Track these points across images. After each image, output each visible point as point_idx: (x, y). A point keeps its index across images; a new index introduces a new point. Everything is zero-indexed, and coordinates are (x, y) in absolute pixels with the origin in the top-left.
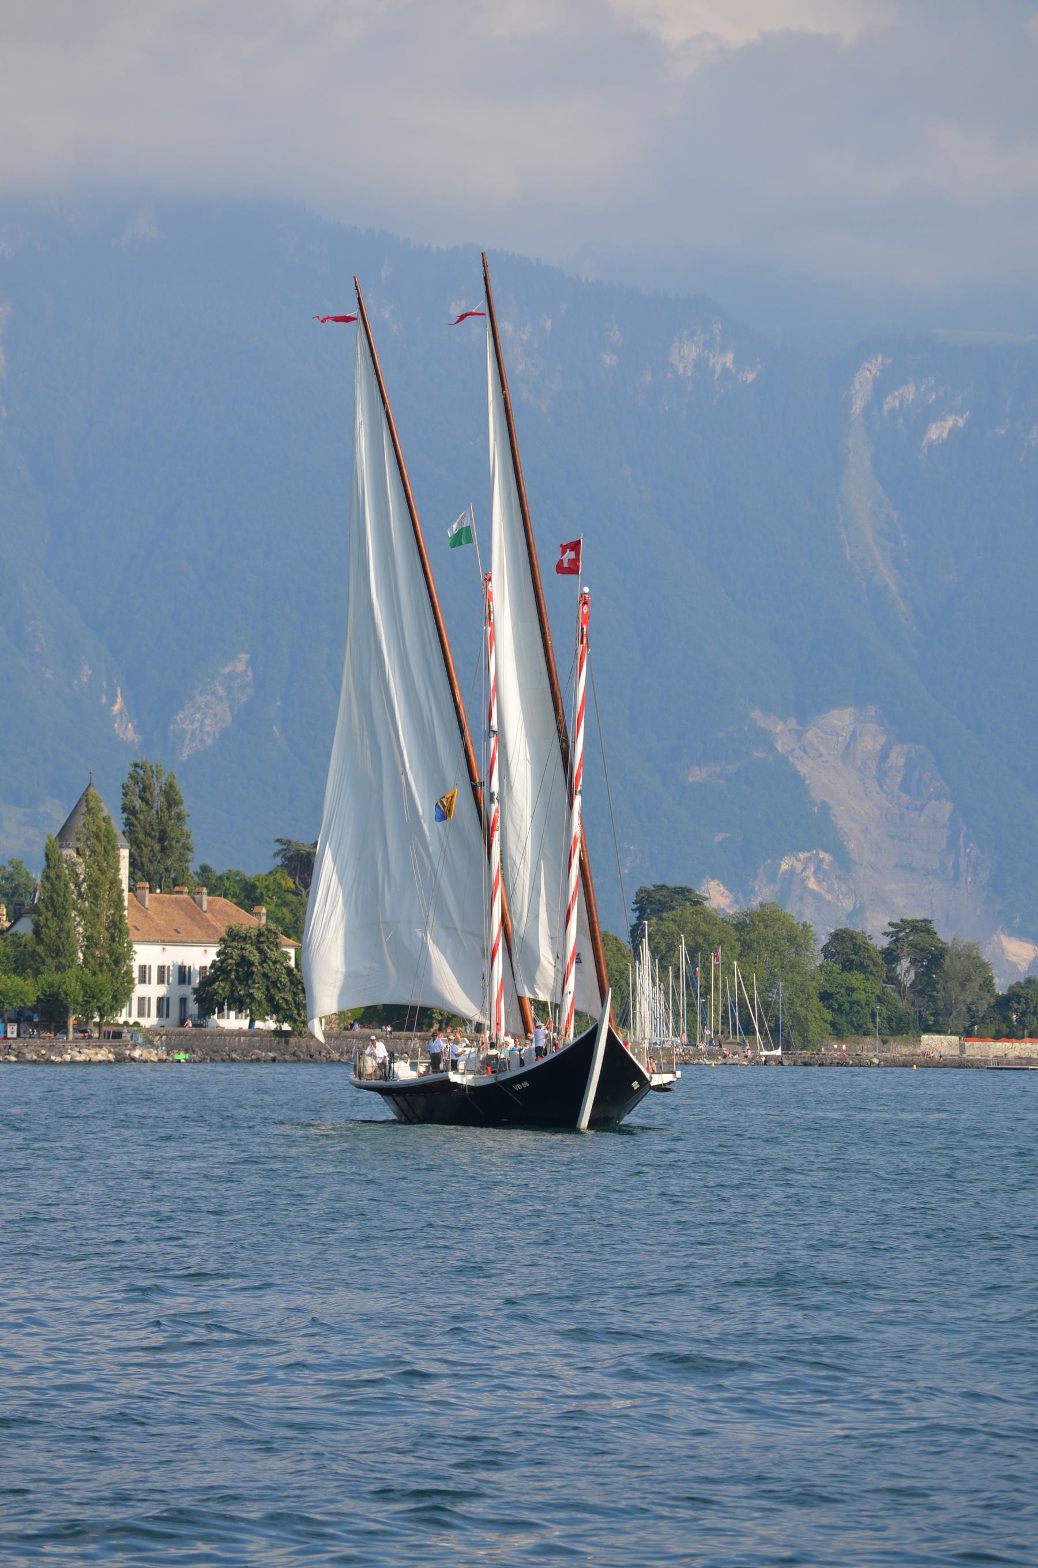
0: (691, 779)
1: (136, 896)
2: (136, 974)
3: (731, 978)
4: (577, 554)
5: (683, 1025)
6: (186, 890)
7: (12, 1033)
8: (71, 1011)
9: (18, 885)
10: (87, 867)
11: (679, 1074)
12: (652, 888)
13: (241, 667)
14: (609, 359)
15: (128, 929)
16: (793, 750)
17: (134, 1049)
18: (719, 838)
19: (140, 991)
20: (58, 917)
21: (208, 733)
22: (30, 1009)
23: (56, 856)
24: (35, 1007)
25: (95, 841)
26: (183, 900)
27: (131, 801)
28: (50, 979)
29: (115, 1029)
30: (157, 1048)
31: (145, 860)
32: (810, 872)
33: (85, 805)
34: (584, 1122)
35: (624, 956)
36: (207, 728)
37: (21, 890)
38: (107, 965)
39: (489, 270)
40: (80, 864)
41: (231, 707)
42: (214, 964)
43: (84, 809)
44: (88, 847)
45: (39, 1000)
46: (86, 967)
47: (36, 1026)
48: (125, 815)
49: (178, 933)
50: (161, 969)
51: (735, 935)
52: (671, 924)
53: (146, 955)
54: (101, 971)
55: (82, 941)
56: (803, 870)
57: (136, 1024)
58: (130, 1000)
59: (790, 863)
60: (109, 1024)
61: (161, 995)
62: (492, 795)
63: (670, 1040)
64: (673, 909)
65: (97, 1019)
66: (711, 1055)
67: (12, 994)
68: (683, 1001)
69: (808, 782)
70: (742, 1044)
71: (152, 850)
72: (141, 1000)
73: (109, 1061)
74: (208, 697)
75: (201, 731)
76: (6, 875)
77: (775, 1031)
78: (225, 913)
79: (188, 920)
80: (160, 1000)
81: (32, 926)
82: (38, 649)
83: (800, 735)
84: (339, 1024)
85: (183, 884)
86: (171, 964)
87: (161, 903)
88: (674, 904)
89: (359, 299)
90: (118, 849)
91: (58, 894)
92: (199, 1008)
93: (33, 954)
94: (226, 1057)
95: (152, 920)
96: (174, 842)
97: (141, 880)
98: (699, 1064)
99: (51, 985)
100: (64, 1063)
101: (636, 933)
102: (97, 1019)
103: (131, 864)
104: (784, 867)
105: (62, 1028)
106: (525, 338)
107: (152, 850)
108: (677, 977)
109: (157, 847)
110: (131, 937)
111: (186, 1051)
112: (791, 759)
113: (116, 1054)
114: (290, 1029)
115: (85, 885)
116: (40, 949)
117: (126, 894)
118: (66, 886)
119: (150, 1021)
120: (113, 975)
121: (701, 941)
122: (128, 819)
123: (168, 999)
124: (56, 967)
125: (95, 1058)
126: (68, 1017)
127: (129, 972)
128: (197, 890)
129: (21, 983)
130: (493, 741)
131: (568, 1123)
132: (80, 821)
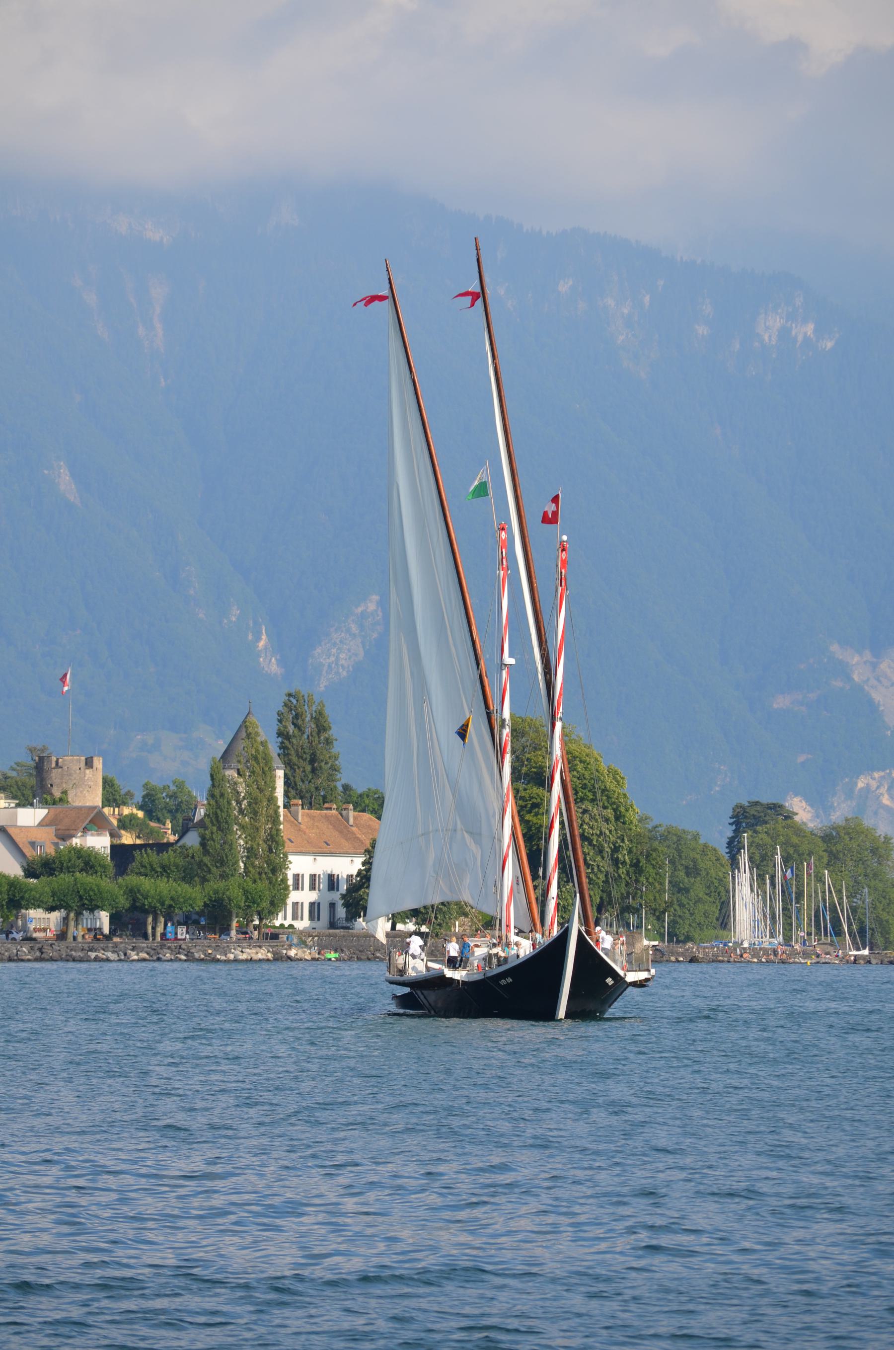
0: (775, 706)
1: (290, 812)
2: (290, 882)
3: (824, 886)
4: (557, 506)
5: (780, 927)
6: (335, 806)
7: (182, 934)
8: (234, 915)
9: (181, 802)
10: (248, 786)
11: (653, 971)
12: (747, 804)
13: (372, 607)
14: (702, 330)
15: (284, 842)
16: (868, 680)
17: (290, 949)
18: (801, 758)
19: (294, 896)
20: (222, 831)
21: (342, 666)
22: (197, 913)
23: (220, 776)
24: (203, 911)
25: (254, 763)
26: (332, 815)
27: (285, 727)
28: (215, 886)
29: (272, 930)
30: (310, 948)
31: (298, 779)
32: (883, 790)
33: (245, 731)
34: (562, 1013)
35: (722, 866)
36: (341, 662)
37: (184, 806)
38: (266, 873)
39: (482, 253)
40: (241, 783)
41: (363, 643)
42: (359, 873)
43: (244, 735)
44: (248, 768)
45: (206, 905)
46: (247, 876)
47: (203, 928)
48: (280, 739)
49: (328, 845)
50: (313, 877)
51: (823, 846)
52: (764, 836)
53: (300, 865)
54: (260, 879)
55: (242, 852)
56: (878, 787)
57: (291, 926)
58: (286, 904)
59: (866, 782)
60: (268, 927)
61: (312, 900)
62: (504, 721)
63: (767, 942)
64: (766, 823)
65: (257, 922)
66: (806, 955)
67: (182, 900)
68: (779, 906)
69: (881, 708)
70: (832, 944)
71: (304, 771)
72: (295, 904)
73: (268, 960)
74: (343, 635)
75: (337, 664)
76: (170, 793)
77: (862, 931)
78: (369, 826)
79: (336, 834)
80: (312, 905)
81: (199, 839)
82: (192, 592)
83: (874, 666)
84: (471, 927)
85: (331, 801)
86: (321, 873)
87: (312, 818)
88: (767, 818)
89: (390, 279)
90: (275, 770)
91: (221, 810)
92: (346, 912)
93: (201, 864)
94: (371, 956)
95: (305, 833)
96: (323, 764)
97: (295, 798)
98: (794, 962)
99: (216, 892)
100: (228, 961)
101: (734, 847)
102: (257, 922)
103: (285, 783)
104: (860, 785)
105: (226, 930)
106: (626, 311)
107: (304, 771)
108: (773, 884)
109: (308, 768)
110: (286, 849)
111: (336, 951)
112: (866, 687)
113: (274, 953)
114: (427, 930)
115: (245, 802)
116: (206, 860)
117: (281, 810)
118: (229, 803)
119: (304, 924)
120: (270, 883)
121: (791, 852)
122: (282, 743)
123: (319, 904)
124: (220, 875)
125: (255, 957)
126: (231, 920)
127: (284, 880)
128: (344, 806)
129: (190, 890)
130: (504, 673)
131: (547, 1014)
132: (241, 745)
